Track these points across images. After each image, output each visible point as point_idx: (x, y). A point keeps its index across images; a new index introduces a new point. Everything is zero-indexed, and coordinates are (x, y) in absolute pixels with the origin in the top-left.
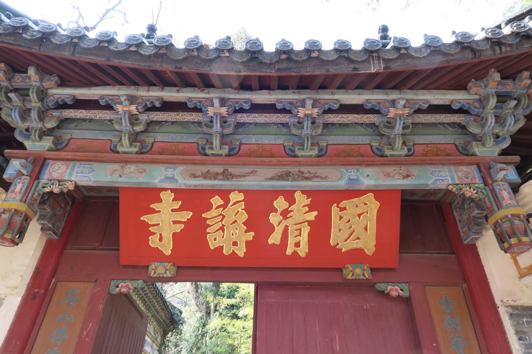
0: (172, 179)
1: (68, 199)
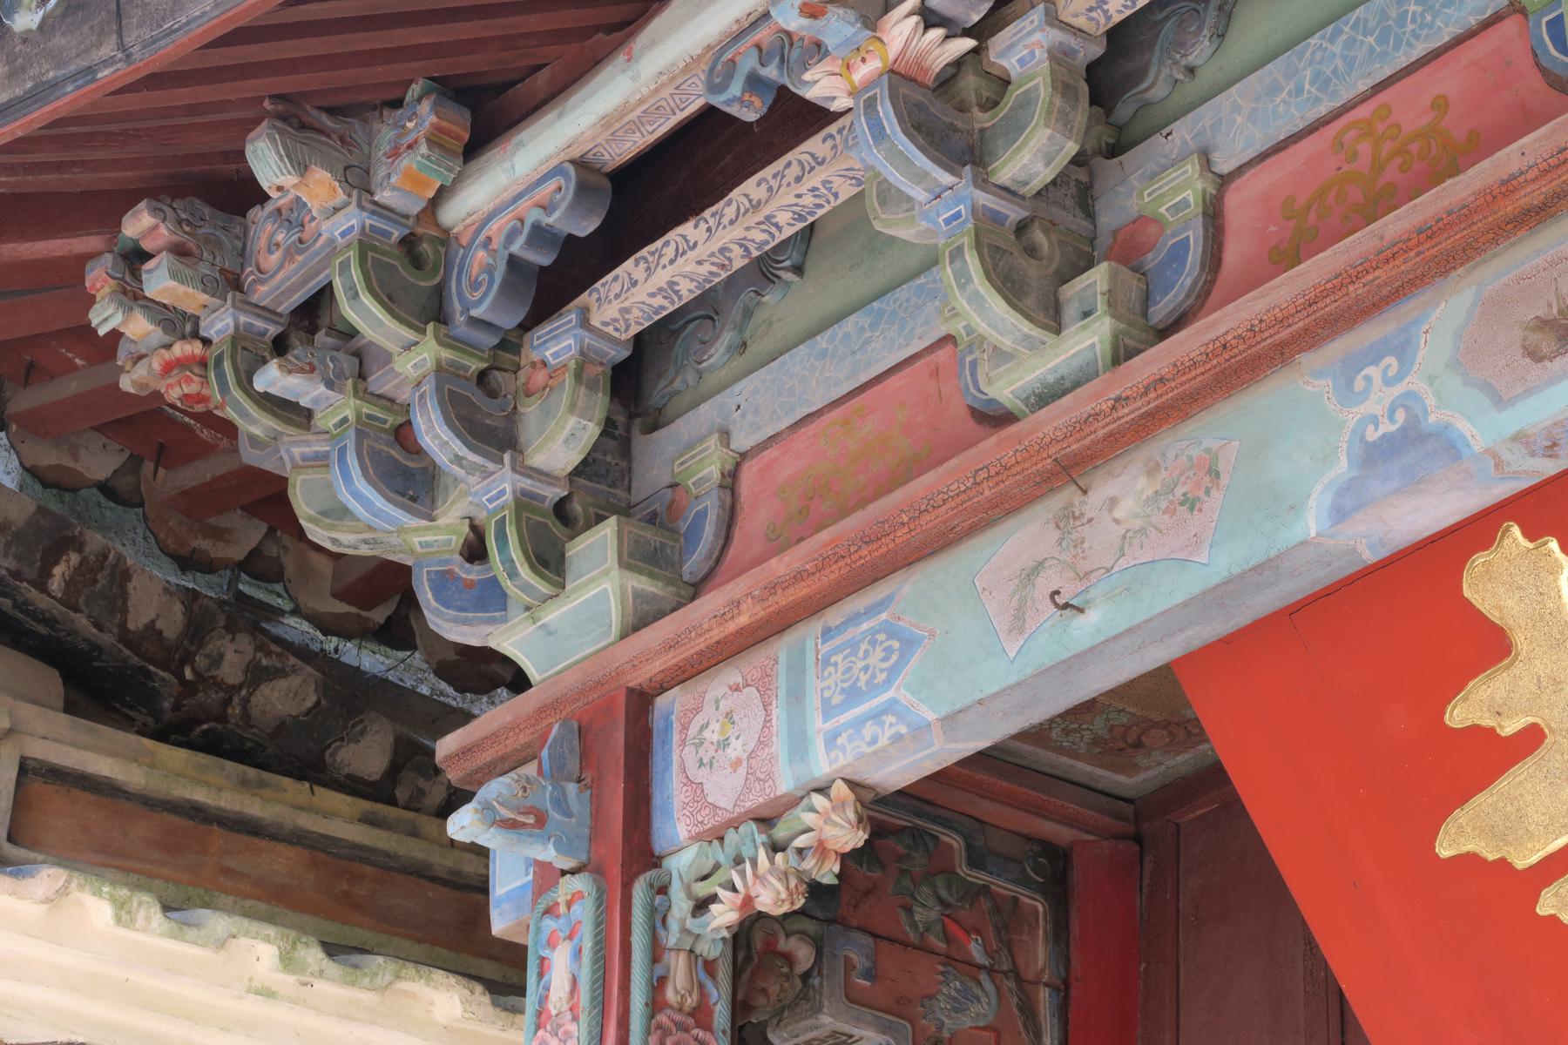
0: (1410, 447)
1: (1004, 887)
